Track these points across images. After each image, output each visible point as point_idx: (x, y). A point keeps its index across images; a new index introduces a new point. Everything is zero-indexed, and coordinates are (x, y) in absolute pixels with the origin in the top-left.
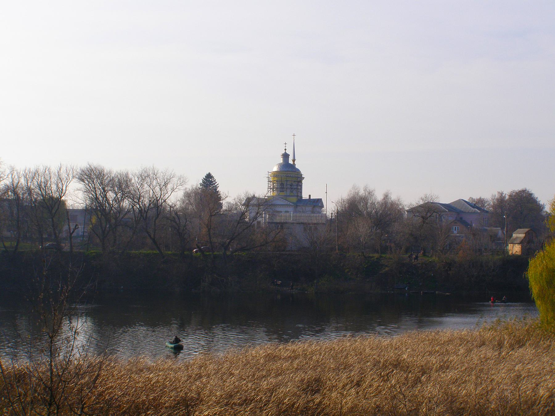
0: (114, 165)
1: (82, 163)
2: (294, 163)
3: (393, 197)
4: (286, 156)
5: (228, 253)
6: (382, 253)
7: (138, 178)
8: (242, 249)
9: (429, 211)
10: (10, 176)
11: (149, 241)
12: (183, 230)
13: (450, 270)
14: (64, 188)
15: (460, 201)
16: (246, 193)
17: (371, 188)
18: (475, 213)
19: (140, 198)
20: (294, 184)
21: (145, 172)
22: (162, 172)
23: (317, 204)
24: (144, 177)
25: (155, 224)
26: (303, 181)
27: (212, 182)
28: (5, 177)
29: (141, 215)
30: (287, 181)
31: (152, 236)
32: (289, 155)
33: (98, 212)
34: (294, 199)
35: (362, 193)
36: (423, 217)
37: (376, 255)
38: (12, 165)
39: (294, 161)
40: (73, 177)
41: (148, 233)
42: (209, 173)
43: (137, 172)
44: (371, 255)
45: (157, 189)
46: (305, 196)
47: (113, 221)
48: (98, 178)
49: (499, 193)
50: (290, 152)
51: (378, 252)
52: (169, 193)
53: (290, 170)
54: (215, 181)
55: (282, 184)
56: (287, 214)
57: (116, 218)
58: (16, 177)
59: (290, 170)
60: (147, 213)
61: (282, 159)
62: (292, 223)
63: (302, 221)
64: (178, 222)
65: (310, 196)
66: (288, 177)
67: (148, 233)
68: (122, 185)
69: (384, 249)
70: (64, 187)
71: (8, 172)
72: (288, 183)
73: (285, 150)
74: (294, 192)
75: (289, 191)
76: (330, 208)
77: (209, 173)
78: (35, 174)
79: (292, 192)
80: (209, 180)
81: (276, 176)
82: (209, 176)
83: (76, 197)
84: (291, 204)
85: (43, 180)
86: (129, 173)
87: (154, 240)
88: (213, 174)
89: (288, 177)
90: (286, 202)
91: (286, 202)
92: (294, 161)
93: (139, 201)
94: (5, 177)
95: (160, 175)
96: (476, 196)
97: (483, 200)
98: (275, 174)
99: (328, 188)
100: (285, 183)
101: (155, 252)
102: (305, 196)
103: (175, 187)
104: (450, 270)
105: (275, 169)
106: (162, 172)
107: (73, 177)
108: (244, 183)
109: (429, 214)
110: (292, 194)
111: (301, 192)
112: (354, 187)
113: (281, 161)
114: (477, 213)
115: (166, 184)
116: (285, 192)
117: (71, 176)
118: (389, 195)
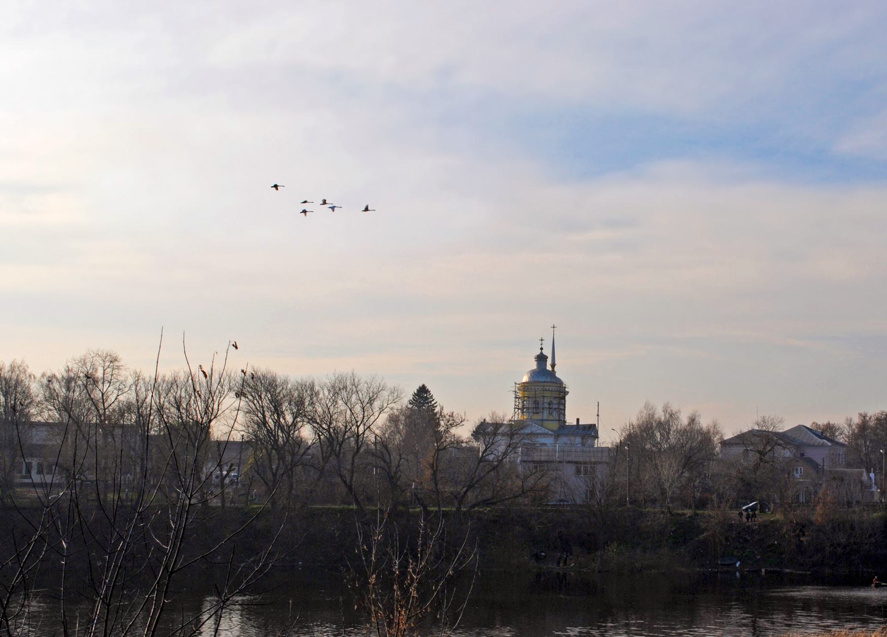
0: (291, 369)
1: (237, 365)
2: (553, 370)
3: (704, 423)
4: (541, 359)
5: (464, 509)
6: (697, 507)
7: (329, 391)
8: (486, 503)
9: (762, 442)
10: (133, 388)
11: (343, 490)
12: (396, 473)
13: (804, 535)
14: (216, 407)
15: (800, 428)
16: (493, 414)
17: (674, 408)
18: (823, 445)
19: (330, 423)
20: (554, 401)
21: (340, 382)
22: (366, 382)
23: (590, 431)
24: (338, 389)
25: (353, 464)
26: (567, 397)
28: (127, 389)
29: (332, 449)
30: (544, 397)
31: (348, 480)
33: (272, 448)
34: (555, 426)
35: (660, 415)
36: (759, 452)
37: (688, 512)
38: (138, 372)
39: (553, 366)
40: (230, 389)
41: (341, 476)
42: (423, 386)
43: (327, 381)
44: (680, 512)
45: (358, 409)
46: (570, 420)
47: (289, 458)
48: (267, 391)
49: (860, 415)
50: (547, 352)
51: (690, 508)
52: (376, 414)
53: (549, 379)
54: (432, 397)
55: (536, 402)
56: (549, 446)
57: (293, 454)
58: (143, 389)
59: (549, 379)
60: (340, 445)
62: (560, 462)
64: (388, 461)
65: (578, 420)
66: (544, 390)
67: (341, 476)
68: (302, 401)
69: (702, 504)
70: (216, 404)
71: (130, 381)
73: (542, 349)
75: (546, 413)
76: (608, 437)
77: (423, 386)
78: (172, 384)
79: (550, 414)
80: (423, 392)
82: (423, 390)
83: (230, 423)
85: (183, 395)
86: (316, 384)
87: (350, 488)
88: (429, 387)
89: (544, 390)
92: (553, 366)
93: (329, 427)
94: (127, 389)
95: (363, 387)
96: (822, 421)
97: (833, 426)
98: (525, 387)
99: (606, 407)
100: (540, 400)
101: (351, 507)
102: (570, 420)
103: (385, 405)
104: (804, 535)
105: (525, 379)
106: (366, 382)
107: (230, 389)
108: (477, 399)
109: (769, 448)
110: (552, 418)
111: (564, 415)
112: (647, 406)
113: (534, 365)
114: (827, 446)
115: (371, 401)
116: (540, 414)
117: (226, 388)
118: (697, 419)
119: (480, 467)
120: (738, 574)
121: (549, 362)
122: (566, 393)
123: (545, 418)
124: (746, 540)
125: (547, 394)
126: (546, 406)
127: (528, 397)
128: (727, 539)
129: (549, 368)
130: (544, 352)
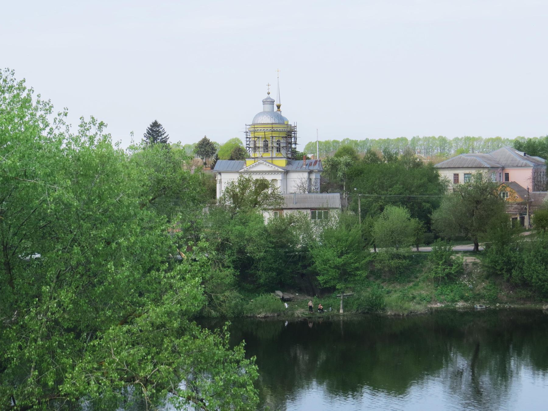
75: (275, 150)
82: (155, 125)
110: (280, 156)
123: (274, 156)
126: (275, 145)
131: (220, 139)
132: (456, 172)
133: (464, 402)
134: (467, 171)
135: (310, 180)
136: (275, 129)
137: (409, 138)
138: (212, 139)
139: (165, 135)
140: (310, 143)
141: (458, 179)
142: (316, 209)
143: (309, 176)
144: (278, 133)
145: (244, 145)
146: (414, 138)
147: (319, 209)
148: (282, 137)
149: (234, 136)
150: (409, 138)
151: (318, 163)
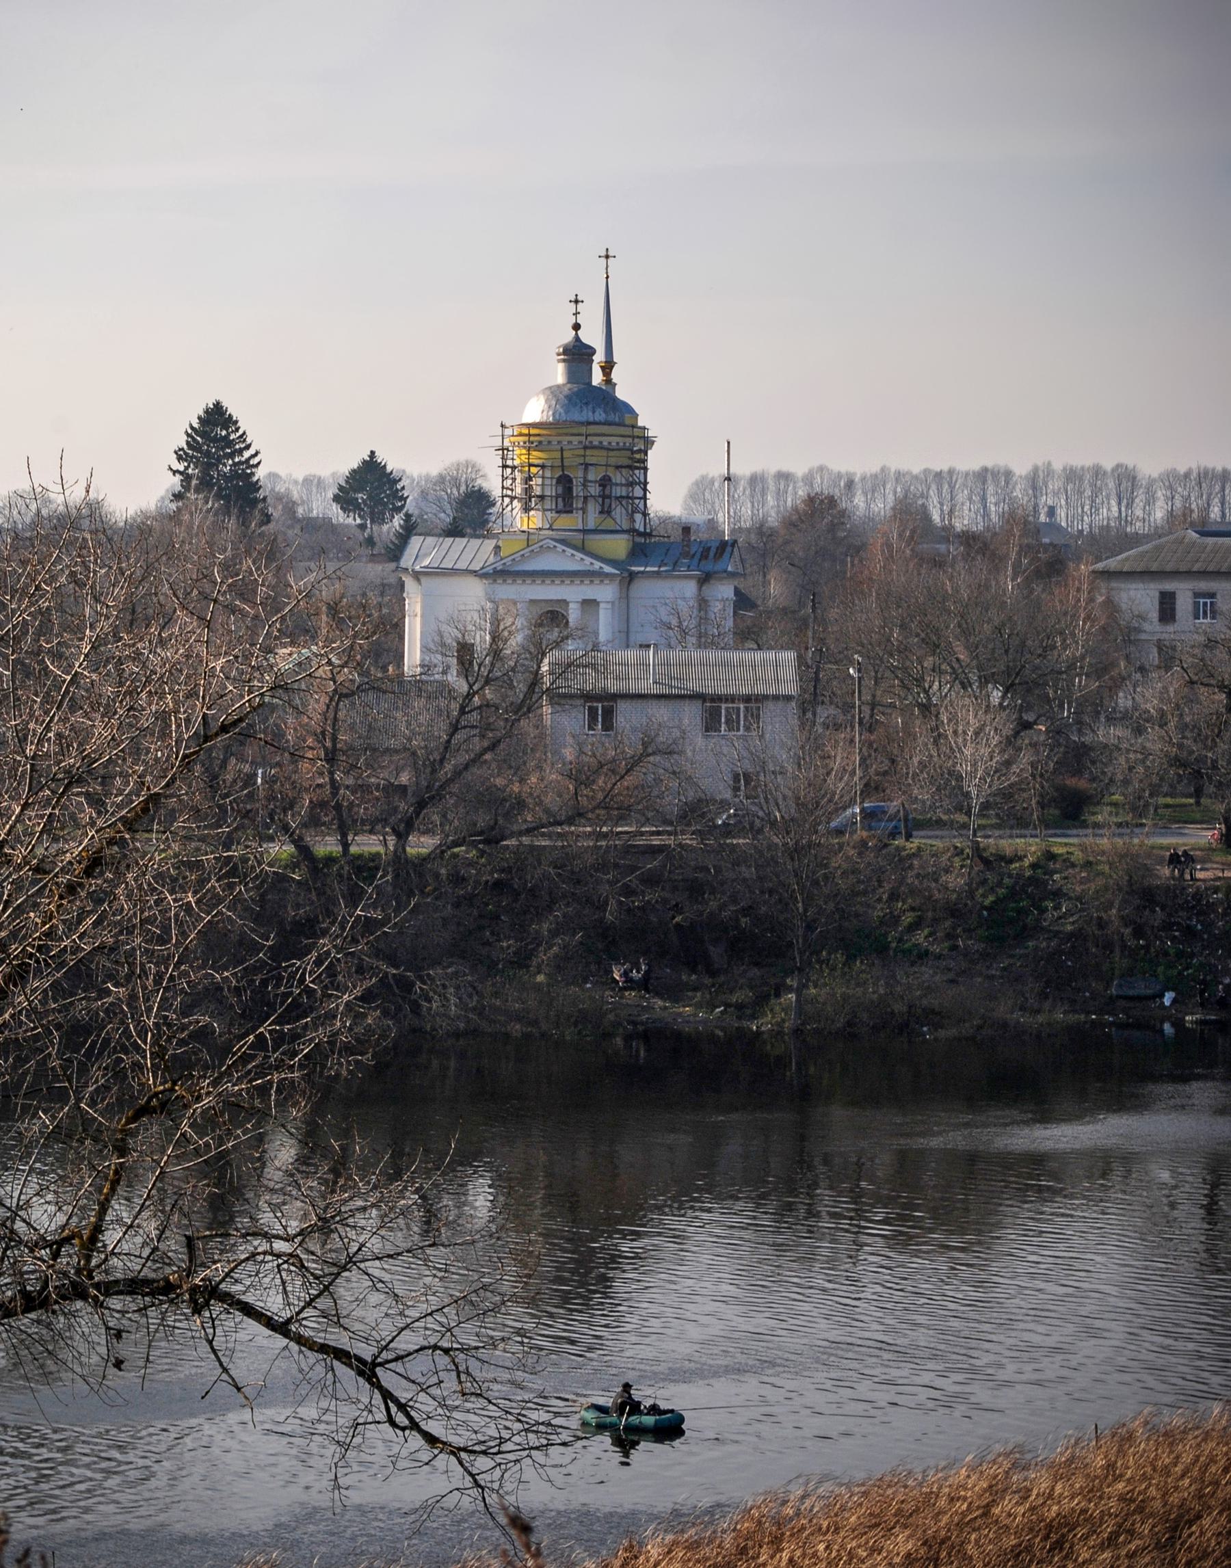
4: (577, 355)
20: (617, 478)
26: (654, 458)
27: (230, 443)
32: (592, 351)
34: (619, 546)
39: (608, 367)
42: (218, 405)
50: (593, 336)
53: (600, 415)
55: (565, 482)
59: (600, 415)
61: (561, 368)
63: (694, 686)
72: (591, 476)
73: (577, 327)
74: (619, 512)
75: (593, 508)
77: (218, 405)
79: (606, 511)
81: (539, 447)
82: (216, 417)
84: (608, 569)
88: (233, 409)
90: (587, 563)
91: (587, 563)
98: (536, 437)
100: (577, 475)
105: (536, 410)
110: (609, 524)
113: (558, 374)
119: (1123, 509)
120: (1167, 1028)
121: (599, 357)
122: (649, 442)
123: (591, 525)
124: (1189, 932)
125: (593, 457)
126: (594, 490)
127: (543, 467)
128: (1138, 932)
129: (597, 378)
130: (586, 337)
131: (416, 462)
132: (1169, 586)
133: (754, 1194)
134: (1203, 585)
135: (703, 603)
136: (596, 441)
137: (1021, 469)
138: (393, 462)
139: (251, 451)
140: (703, 477)
141: (1173, 610)
142: (718, 698)
143: (700, 589)
144: (604, 453)
145: (493, 483)
146: (1036, 469)
147: (731, 699)
148: (617, 467)
149: (462, 457)
150: (1021, 469)
151: (729, 549)
